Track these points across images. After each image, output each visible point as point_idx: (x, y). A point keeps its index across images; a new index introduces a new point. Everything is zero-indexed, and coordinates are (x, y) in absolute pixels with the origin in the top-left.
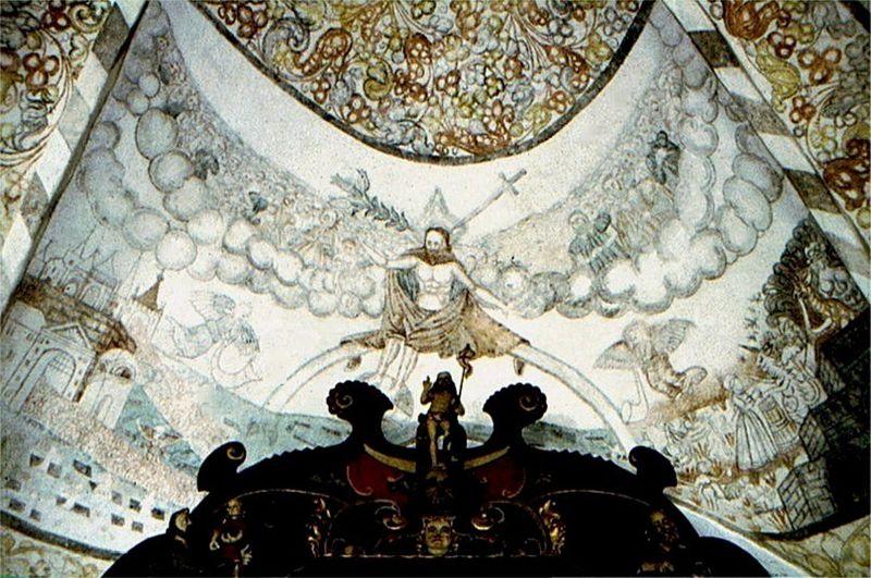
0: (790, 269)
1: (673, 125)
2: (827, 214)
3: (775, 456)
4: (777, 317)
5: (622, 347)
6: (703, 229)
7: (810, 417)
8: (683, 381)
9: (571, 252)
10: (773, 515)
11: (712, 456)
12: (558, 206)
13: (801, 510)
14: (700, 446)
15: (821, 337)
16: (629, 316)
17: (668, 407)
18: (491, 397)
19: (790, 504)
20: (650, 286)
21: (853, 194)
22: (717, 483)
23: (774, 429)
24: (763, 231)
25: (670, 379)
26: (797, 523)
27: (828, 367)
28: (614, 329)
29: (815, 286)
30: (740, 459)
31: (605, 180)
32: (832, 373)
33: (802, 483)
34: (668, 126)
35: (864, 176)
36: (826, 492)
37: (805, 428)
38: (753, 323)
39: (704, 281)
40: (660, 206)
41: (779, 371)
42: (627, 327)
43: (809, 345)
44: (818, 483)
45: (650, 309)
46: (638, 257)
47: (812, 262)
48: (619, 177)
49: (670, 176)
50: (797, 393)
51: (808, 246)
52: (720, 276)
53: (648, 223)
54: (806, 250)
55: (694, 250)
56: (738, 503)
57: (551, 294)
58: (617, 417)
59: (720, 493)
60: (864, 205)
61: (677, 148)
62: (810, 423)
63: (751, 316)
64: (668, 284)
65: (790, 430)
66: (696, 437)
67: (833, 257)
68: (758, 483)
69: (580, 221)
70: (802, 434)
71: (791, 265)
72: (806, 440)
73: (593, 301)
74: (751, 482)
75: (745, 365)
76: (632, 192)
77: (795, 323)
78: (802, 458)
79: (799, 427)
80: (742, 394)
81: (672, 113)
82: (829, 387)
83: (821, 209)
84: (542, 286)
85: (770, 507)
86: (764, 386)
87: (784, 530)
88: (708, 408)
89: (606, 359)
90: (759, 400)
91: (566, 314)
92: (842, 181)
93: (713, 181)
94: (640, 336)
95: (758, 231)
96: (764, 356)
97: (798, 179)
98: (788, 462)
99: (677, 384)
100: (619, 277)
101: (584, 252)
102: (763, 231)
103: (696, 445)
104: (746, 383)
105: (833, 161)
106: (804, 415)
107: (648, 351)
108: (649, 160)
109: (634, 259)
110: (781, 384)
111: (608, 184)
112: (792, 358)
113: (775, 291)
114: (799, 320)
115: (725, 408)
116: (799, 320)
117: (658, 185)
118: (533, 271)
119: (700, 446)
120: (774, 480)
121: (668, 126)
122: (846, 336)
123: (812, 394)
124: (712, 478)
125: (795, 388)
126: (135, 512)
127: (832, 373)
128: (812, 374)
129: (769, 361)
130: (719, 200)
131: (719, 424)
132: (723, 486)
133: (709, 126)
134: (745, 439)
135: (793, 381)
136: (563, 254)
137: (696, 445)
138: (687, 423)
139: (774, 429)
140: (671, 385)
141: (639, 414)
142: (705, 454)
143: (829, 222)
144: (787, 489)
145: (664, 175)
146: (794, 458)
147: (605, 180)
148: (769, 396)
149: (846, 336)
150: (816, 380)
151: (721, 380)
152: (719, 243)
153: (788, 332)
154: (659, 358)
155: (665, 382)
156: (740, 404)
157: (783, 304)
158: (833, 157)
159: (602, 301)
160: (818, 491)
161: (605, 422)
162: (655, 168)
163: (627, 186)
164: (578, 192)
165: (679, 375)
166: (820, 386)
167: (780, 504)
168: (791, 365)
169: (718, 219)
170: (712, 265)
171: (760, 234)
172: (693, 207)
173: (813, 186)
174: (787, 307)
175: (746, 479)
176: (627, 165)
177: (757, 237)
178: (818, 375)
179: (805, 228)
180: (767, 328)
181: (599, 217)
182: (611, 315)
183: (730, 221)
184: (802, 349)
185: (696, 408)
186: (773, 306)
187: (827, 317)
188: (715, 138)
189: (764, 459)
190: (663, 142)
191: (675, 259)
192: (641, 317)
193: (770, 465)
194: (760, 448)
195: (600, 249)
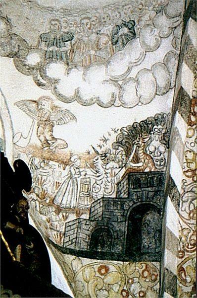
0: (139, 131)
1: (143, 23)
3: (74, 208)
5: (34, 105)
6: (114, 81)
8: (54, 143)
9: (41, 37)
10: (57, 233)
11: (44, 188)
12: (51, 9)
13: (72, 240)
14: (42, 178)
16: (48, 93)
17: (39, 150)
20: (67, 86)
22: (39, 202)
24: (142, 103)
25: (48, 138)
26: (67, 244)
27: (125, 184)
28: (36, 93)
29: (146, 145)
30: (57, 198)
31: (85, 18)
32: (125, 187)
34: (139, 21)
38: (105, 140)
39: (96, 103)
40: (103, 54)
41: (102, 170)
42: (44, 97)
43: (124, 168)
44: (86, 232)
46: (72, 68)
47: (153, 133)
48: (94, 23)
49: (120, 43)
50: (103, 186)
53: (90, 56)
54: (155, 127)
56: (44, 218)
57: (16, 50)
59: (38, 208)
61: (135, 34)
62: (100, 203)
63: (107, 137)
64: (77, 92)
65: (89, 200)
67: (167, 141)
68: (58, 215)
69: (57, 26)
71: (143, 128)
72: (93, 209)
73: (35, 71)
76: (94, 35)
78: (86, 216)
79: (93, 201)
80: (77, 168)
81: (146, 17)
82: (120, 193)
83: (182, 116)
84: (14, 42)
85: (58, 229)
86: (89, 172)
87: (59, 244)
88: (57, 164)
89: (23, 104)
91: (17, 66)
93: (139, 63)
94: (47, 106)
95: (140, 102)
96: (100, 159)
98: (78, 214)
99: (49, 142)
100: (55, 70)
101: (47, 43)
102: (142, 103)
103: (40, 177)
104: (83, 165)
106: (99, 198)
107: (46, 117)
108: (116, 28)
109: (70, 67)
110: (98, 176)
111: (85, 21)
114: (128, 155)
115: (64, 169)
116: (128, 155)
117: (110, 42)
118: (14, 31)
119: (42, 178)
120: (67, 218)
121: (139, 21)
122: (144, 176)
123: (109, 190)
124: (38, 199)
125: (104, 182)
126: (100, 98)
127: (125, 187)
129: (100, 162)
130: (133, 74)
131: (57, 174)
132: (41, 206)
133: (160, 39)
134: (64, 190)
135: (105, 178)
136: (36, 35)
137: (40, 177)
138: (43, 163)
140: (47, 140)
141: (23, 143)
142: (42, 184)
143: (180, 124)
144: (70, 226)
145: (117, 41)
146: (82, 214)
147: (85, 18)
148: (89, 178)
149: (144, 176)
150: (116, 186)
151: (71, 155)
152: (117, 92)
153: (119, 156)
154: (48, 123)
157: (126, 142)
159: (39, 74)
161: (4, 135)
162: (116, 34)
163: (94, 31)
164: (66, 11)
167: (64, 231)
168: (109, 171)
169: (126, 81)
170: (106, 100)
171: (140, 104)
172: (118, 67)
176: (103, 20)
179: (163, 117)
180: (111, 147)
181: (68, 33)
182: (39, 84)
183: (130, 88)
184: (119, 167)
186: (120, 140)
188: (158, 46)
190: (130, 26)
192: (54, 97)
195: (57, 49)
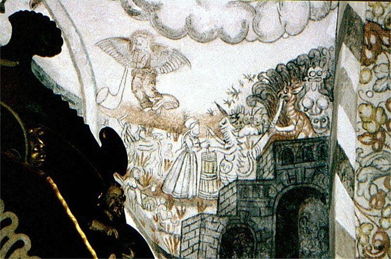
2: (352, 56)
3: (194, 197)
4: (256, 101)
5: (126, 44)
7: (235, 184)
8: (158, 101)
13: (193, 246)
15: (279, 135)
16: (145, 25)
18: (21, 11)
19: (187, 237)
21: (369, 54)
22: (141, 191)
23: (204, 177)
25: (150, 93)
26: (185, 254)
27: (269, 158)
29: (298, 98)
30: (167, 182)
32: (269, 164)
33: (202, 227)
35: (384, 47)
36: (216, 243)
37: (226, 189)
38: (236, 94)
41: (233, 139)
43: (266, 135)
45: (164, 30)
50: (235, 162)
51: (314, 68)
52: (233, 44)
54: (311, 69)
55: (227, 12)
58: (93, 95)
60: (371, 66)
62: (232, 188)
64: (189, 22)
66: (144, 148)
68: (170, 208)
70: (221, 193)
71: (292, 72)
74: (165, 204)
75: (210, 119)
77: (268, 114)
78: (212, 210)
79: (222, 186)
80: (195, 137)
82: (262, 172)
83: (351, 49)
86: (214, 143)
87: (173, 254)
88: (164, 132)
89: (108, 44)
90: (204, 150)
92: (369, 40)
94: (144, 45)
96: (228, 121)
97: (351, 18)
98: (201, 206)
99: (151, 100)
104: (203, 132)
105: (373, 22)
106: (231, 180)
110: (228, 149)
112: (249, 136)
113: (267, 82)
114: (271, 113)
115: (176, 140)
116: (271, 113)
124: (139, 185)
125: (237, 158)
128: (255, 157)
129: (229, 127)
134: (178, 171)
139: (204, 177)
140: (147, 98)
141: (111, 103)
146: (206, 207)
150: (255, 162)
151: (185, 118)
152: (250, 20)
153: (258, 116)
154: (148, 72)
155: (144, 93)
156: (189, 144)
157: (267, 94)
158: (375, 20)
160: (211, 240)
165: (157, 94)
166: (255, 167)
167: (179, 233)
168: (244, 140)
170: (233, 32)
171: (286, 35)
173: (357, 30)
174: (269, 98)
175: (163, 201)
177: (282, 36)
178: (259, 159)
179: (321, 54)
182: (131, 13)
184: (260, 134)
185: (155, 126)
186: (259, 92)
187: (292, 123)
189: (184, 194)
191: (207, 8)
192: (154, 32)
193: (187, 200)
194: (185, 185)
